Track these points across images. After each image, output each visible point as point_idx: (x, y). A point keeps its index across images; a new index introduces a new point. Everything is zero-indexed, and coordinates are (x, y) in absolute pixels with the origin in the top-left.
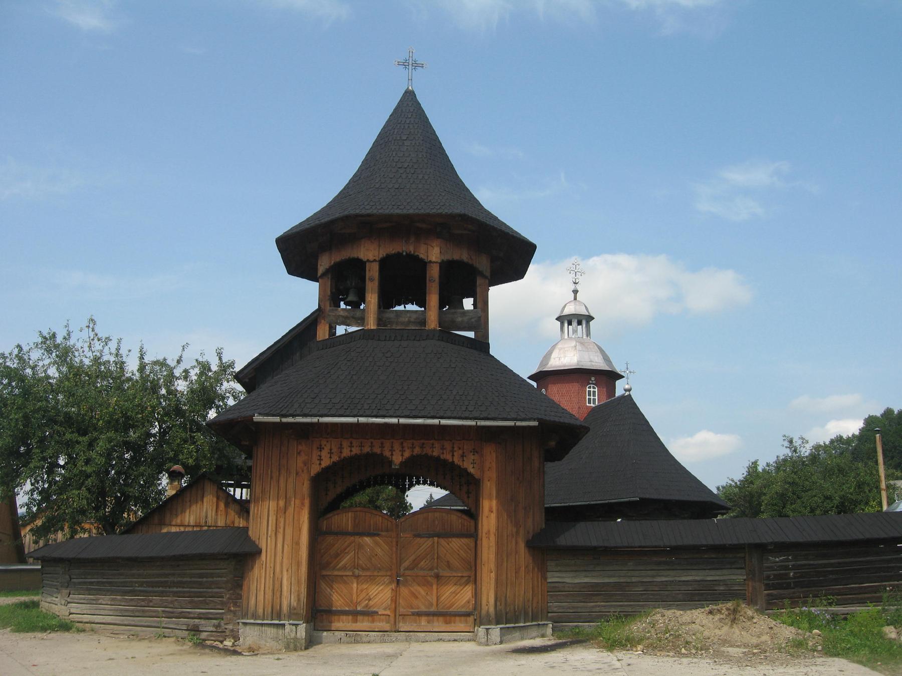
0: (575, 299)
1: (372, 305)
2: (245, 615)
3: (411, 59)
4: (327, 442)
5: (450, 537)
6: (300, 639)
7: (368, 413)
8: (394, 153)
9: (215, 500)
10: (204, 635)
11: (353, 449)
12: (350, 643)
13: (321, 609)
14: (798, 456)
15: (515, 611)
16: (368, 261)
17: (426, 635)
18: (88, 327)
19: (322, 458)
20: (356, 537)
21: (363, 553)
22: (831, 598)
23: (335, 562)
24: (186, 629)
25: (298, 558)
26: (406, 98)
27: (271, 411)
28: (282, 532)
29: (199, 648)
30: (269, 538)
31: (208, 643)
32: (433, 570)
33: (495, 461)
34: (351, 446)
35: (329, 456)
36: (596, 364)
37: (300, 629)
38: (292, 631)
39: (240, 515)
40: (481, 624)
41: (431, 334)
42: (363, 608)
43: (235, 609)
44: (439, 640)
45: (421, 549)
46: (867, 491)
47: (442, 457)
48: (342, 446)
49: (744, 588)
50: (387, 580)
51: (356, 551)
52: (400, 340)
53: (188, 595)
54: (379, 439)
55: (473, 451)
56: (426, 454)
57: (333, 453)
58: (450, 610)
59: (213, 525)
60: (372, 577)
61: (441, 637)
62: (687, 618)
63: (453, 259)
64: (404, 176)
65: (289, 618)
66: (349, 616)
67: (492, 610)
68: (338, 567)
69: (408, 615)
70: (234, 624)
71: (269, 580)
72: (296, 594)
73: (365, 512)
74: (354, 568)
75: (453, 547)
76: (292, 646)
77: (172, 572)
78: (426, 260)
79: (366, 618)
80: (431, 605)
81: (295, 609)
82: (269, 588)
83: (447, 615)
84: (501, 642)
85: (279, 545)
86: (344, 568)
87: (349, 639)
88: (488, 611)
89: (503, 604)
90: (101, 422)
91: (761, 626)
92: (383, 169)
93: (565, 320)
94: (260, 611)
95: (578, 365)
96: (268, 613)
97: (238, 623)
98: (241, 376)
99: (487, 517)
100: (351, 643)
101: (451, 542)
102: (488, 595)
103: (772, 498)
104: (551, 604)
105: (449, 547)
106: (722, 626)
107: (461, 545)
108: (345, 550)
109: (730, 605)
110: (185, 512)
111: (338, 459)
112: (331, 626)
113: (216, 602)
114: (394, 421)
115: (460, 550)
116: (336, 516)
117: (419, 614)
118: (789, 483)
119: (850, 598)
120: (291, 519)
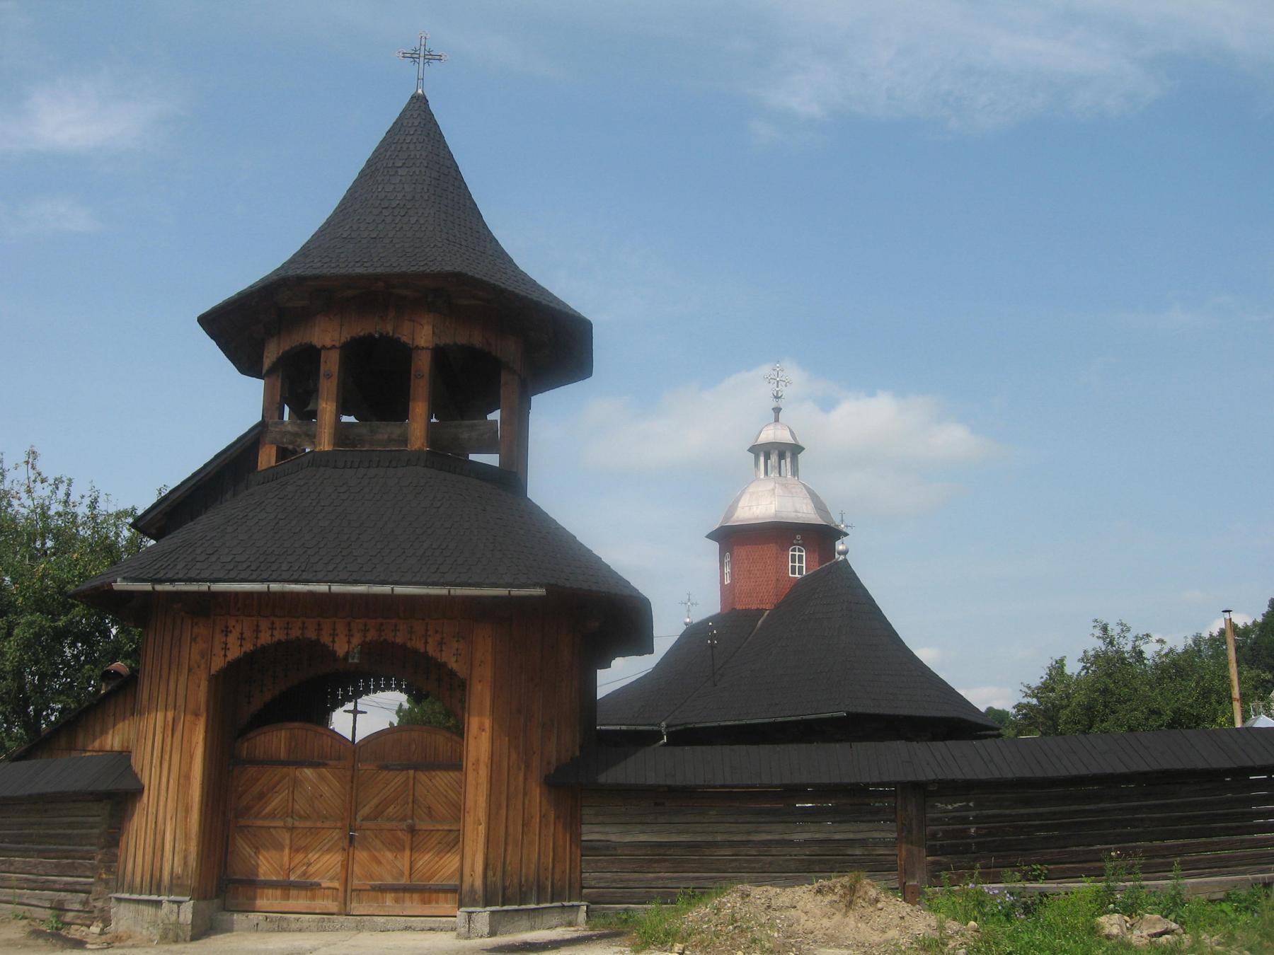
0: (777, 420)
1: (328, 414)
3: (423, 48)
5: (434, 770)
6: (183, 924)
7: (285, 576)
8: (380, 187)
11: (275, 633)
12: (272, 931)
13: (235, 877)
14: (35, 601)
15: (521, 886)
16: (324, 347)
17: (387, 920)
18: (27, 462)
19: (229, 645)
20: (291, 767)
22: (1038, 869)
24: (49, 906)
27: (141, 573)
28: (168, 759)
30: (153, 769)
32: (406, 820)
36: (804, 515)
37: (183, 910)
38: (171, 912)
42: (299, 876)
43: (107, 877)
44: (407, 928)
45: (389, 787)
46: (1213, 701)
47: (409, 645)
49: (893, 853)
50: (336, 834)
51: (291, 789)
56: (385, 640)
58: (430, 883)
61: (409, 925)
62: (785, 899)
65: (171, 892)
66: (276, 889)
67: (479, 883)
68: (263, 813)
75: (439, 787)
76: (171, 934)
78: (411, 346)
79: (303, 893)
80: (402, 874)
81: (179, 878)
83: (425, 891)
84: (492, 934)
89: (499, 873)
90: (21, 599)
91: (890, 914)
92: (360, 210)
93: (763, 451)
95: (776, 516)
97: (111, 898)
98: (140, 524)
99: (476, 738)
100: (273, 931)
101: (434, 778)
103: (1073, 713)
104: (588, 874)
105: (430, 783)
106: (834, 914)
108: (273, 789)
109: (846, 880)
111: (252, 648)
114: (323, 588)
115: (450, 792)
116: (263, 735)
117: (383, 889)
119: (1068, 868)
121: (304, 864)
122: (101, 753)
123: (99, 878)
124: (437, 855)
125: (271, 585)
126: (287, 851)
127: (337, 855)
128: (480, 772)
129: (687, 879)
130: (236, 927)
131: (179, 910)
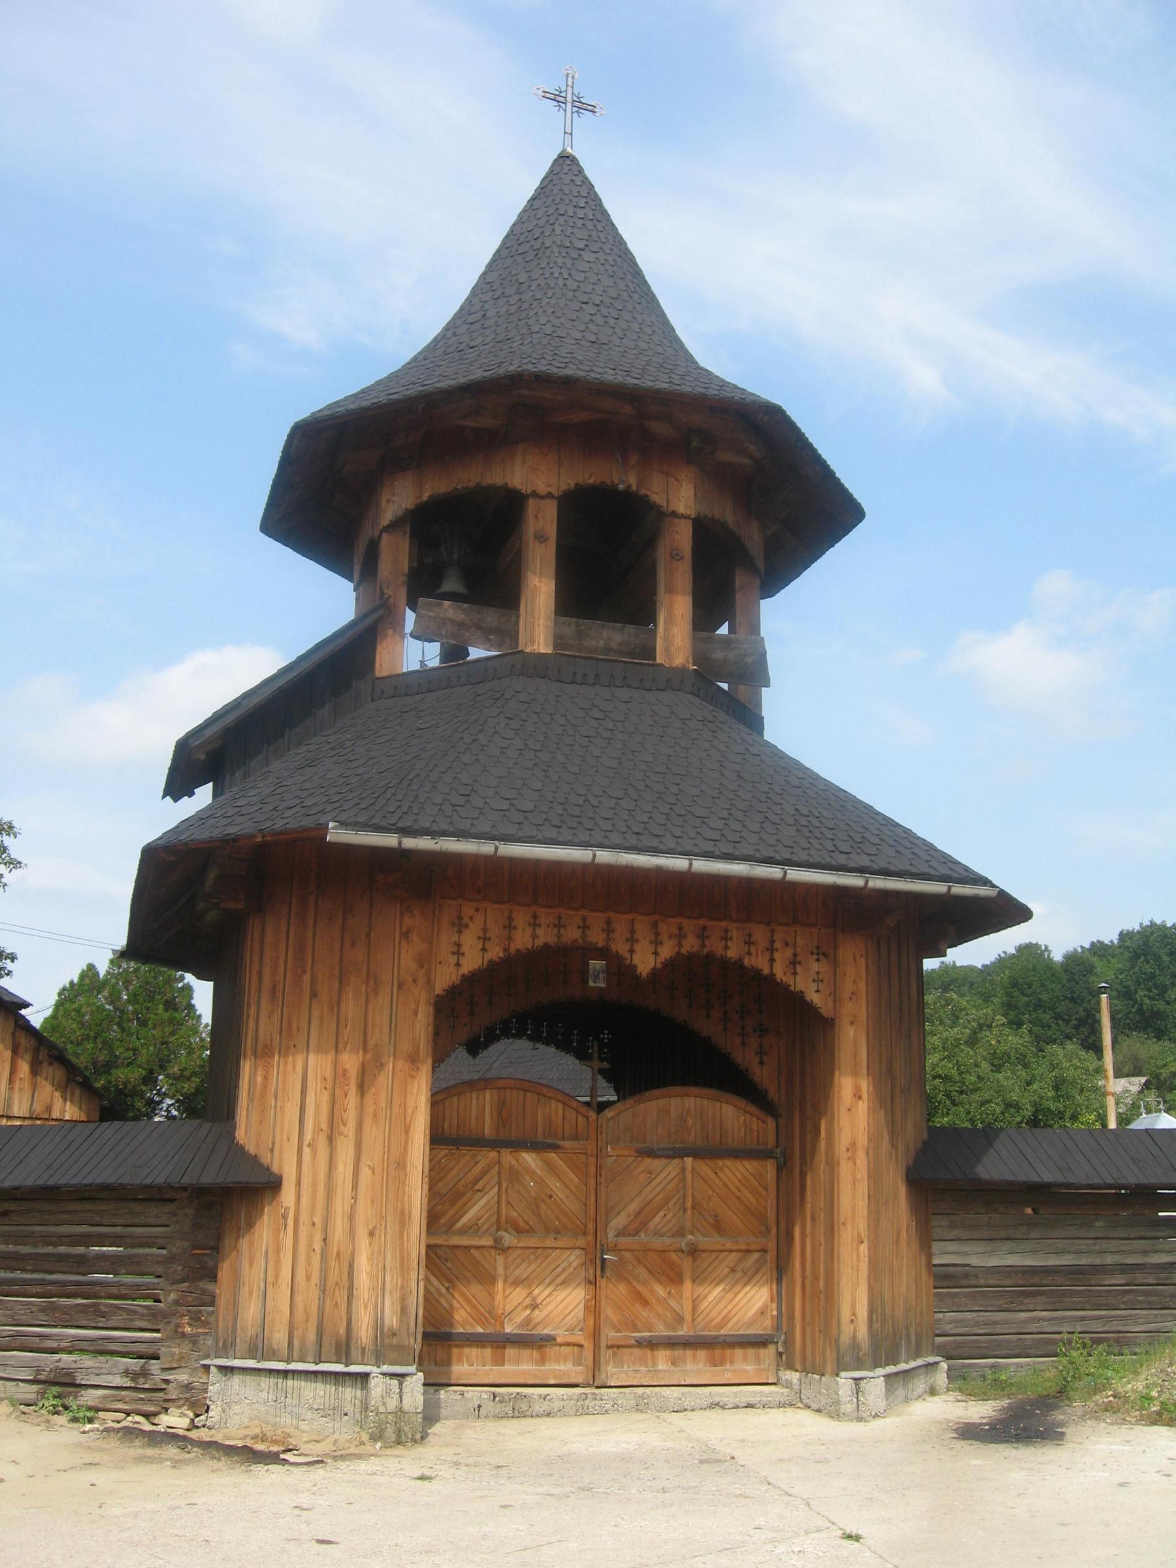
1: (542, 598)
2: (225, 1346)
4: (477, 910)
10: (91, 1397)
11: (540, 932)
16: (535, 494)
19: (465, 949)
20: (503, 1150)
23: (452, 1212)
24: (32, 1378)
25: (403, 1202)
28: (352, 1135)
29: (137, 1443)
30: (307, 1151)
33: (864, 977)
34: (535, 925)
35: (480, 946)
38: (389, 1392)
41: (672, 680)
42: (521, 1326)
44: (714, 1405)
45: (654, 1184)
47: (746, 962)
48: (513, 924)
50: (574, 1258)
53: (39, 1289)
54: (602, 911)
55: (815, 951)
57: (489, 939)
58: (722, 1332)
60: (539, 1251)
61: (717, 1399)
63: (713, 516)
66: (484, 1347)
67: (863, 1332)
68: (459, 1225)
69: (626, 1346)
73: (525, 1091)
74: (498, 1229)
76: (390, 1433)
78: (665, 510)
79: (526, 1352)
80: (680, 1319)
81: (394, 1334)
82: (308, 1278)
85: (341, 1167)
86: (473, 1228)
87: (498, 1408)
88: (854, 1337)
94: (279, 1337)
100: (505, 1417)
101: (721, 1169)
102: (854, 1298)
108: (475, 1184)
111: (501, 955)
113: (135, 1312)
114: (679, 863)
115: (742, 1188)
116: (456, 1098)
117: (652, 1344)
118: (940, 1076)
122: (38, 1122)
123: (176, 1332)
125: (598, 853)
126: (500, 1285)
127: (578, 1291)
128: (858, 1161)
130: (443, 1413)
131: (401, 1390)
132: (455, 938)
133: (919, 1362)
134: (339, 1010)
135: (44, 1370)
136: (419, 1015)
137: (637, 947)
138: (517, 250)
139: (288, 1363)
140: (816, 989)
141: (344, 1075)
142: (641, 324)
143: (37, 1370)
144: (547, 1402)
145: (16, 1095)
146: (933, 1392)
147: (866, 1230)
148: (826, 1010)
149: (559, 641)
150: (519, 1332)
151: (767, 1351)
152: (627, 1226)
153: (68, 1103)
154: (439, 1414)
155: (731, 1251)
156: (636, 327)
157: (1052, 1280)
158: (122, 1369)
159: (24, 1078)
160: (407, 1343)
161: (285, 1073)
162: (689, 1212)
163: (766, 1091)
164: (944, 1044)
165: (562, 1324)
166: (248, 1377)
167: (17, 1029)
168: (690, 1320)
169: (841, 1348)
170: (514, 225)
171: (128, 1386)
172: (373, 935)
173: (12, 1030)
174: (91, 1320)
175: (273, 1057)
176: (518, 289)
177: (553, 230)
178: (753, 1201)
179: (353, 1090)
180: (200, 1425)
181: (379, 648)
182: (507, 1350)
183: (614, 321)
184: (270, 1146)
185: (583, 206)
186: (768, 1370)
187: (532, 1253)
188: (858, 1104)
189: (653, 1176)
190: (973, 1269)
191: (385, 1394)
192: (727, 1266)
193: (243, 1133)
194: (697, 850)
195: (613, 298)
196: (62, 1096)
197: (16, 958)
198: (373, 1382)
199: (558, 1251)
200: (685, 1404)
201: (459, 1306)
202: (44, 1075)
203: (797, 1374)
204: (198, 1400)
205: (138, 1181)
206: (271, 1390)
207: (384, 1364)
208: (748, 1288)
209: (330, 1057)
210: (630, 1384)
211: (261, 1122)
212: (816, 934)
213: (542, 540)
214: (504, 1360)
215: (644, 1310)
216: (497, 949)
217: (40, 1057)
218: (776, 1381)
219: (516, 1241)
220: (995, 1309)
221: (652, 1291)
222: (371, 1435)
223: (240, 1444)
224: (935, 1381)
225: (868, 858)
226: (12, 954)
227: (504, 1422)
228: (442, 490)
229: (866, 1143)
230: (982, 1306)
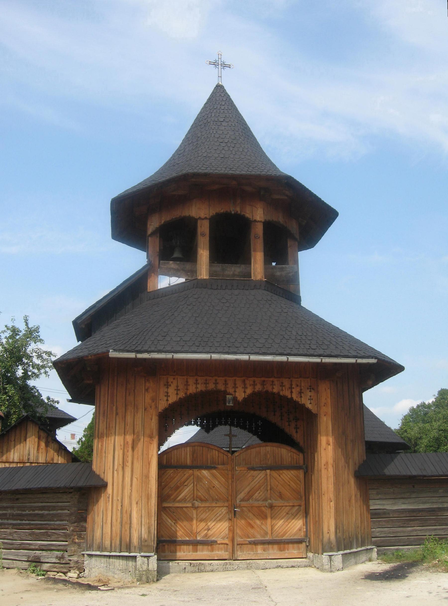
1: (204, 258)
4: (174, 379)
9: (36, 440)
10: (45, 567)
11: (199, 386)
13: (162, 539)
16: (200, 218)
19: (170, 394)
20: (194, 470)
21: (201, 486)
24: (26, 560)
25: (148, 490)
26: (218, 90)
28: (130, 466)
29: (50, 583)
30: (115, 472)
31: (51, 574)
32: (267, 501)
34: (196, 383)
35: (176, 393)
38: (143, 563)
39: (59, 452)
40: (324, 551)
41: (257, 285)
42: (203, 537)
44: (278, 567)
47: (281, 393)
48: (188, 384)
50: (224, 510)
52: (231, 289)
53: (28, 527)
54: (223, 377)
55: (309, 388)
57: (179, 390)
58: (284, 538)
59: (35, 462)
60: (210, 508)
61: (279, 564)
63: (273, 220)
64: (226, 148)
65: (141, 550)
66: (189, 545)
67: (333, 537)
68: (179, 498)
70: (79, 556)
71: (117, 513)
72: (147, 526)
73: (202, 447)
74: (194, 500)
76: (144, 578)
77: (12, 505)
79: (206, 547)
80: (266, 533)
81: (146, 541)
82: (117, 521)
85: (127, 479)
86: (184, 500)
87: (193, 569)
94: (107, 543)
96: (115, 546)
100: (195, 572)
101: (282, 474)
102: (329, 523)
107: (291, 477)
110: (10, 451)
111: (184, 396)
112: (176, 555)
113: (60, 535)
114: (245, 357)
115: (291, 482)
117: (255, 543)
118: (442, 430)
120: (140, 453)
121: (205, 530)
123: (73, 541)
124: (286, 521)
126: (195, 521)
128: (329, 470)
129: (430, 530)
132: (166, 390)
133: (363, 548)
134: (125, 419)
135: (30, 557)
136: (153, 420)
137: (237, 390)
138: (198, 124)
139: (110, 553)
140: (310, 403)
141: (127, 444)
142: (243, 148)
143: (28, 557)
144: (211, 566)
145: (40, 455)
146: (370, 560)
147: (333, 497)
148: (314, 410)
149: (211, 274)
150: (203, 539)
151: (302, 545)
152: (244, 497)
153: (60, 457)
154: (170, 571)
155: (286, 506)
156: (241, 150)
157: (421, 514)
158: (55, 556)
159: (43, 448)
160: (151, 544)
161: (108, 444)
162: (269, 491)
163: (299, 443)
164: (444, 417)
165: (220, 536)
166: (97, 558)
167: (40, 430)
168: (270, 533)
169: (324, 543)
170: (198, 114)
171: (58, 562)
172: (136, 391)
173: (38, 431)
174: (45, 538)
175: (104, 438)
176: (197, 140)
177: (212, 115)
178: (295, 486)
179: (130, 449)
180: (81, 576)
181: (149, 281)
182: (198, 546)
183: (232, 148)
184: (103, 471)
185: (224, 104)
186: (303, 553)
187: (207, 509)
188: (328, 447)
189: (254, 478)
190: (387, 510)
191: (142, 563)
192: (285, 512)
193: (95, 466)
194: (252, 352)
195: (233, 139)
196: (57, 455)
197: (59, 403)
198: (138, 559)
199: (217, 508)
200: (267, 566)
201: (179, 530)
202: (50, 447)
203: (312, 554)
204: (81, 567)
205: (55, 486)
206: (105, 563)
207: (142, 552)
208: (294, 521)
209: (123, 437)
210: (247, 559)
211: (100, 462)
212: (309, 381)
213: (203, 235)
214: (197, 550)
215: (252, 530)
216: (182, 393)
217: (49, 440)
218: (306, 557)
219: (200, 504)
220: (397, 526)
221: (255, 523)
222: (137, 579)
223: (86, 583)
224: (371, 556)
225: (323, 350)
226: (58, 401)
227: (194, 574)
228: (168, 219)
229: (332, 462)
230: (391, 525)
